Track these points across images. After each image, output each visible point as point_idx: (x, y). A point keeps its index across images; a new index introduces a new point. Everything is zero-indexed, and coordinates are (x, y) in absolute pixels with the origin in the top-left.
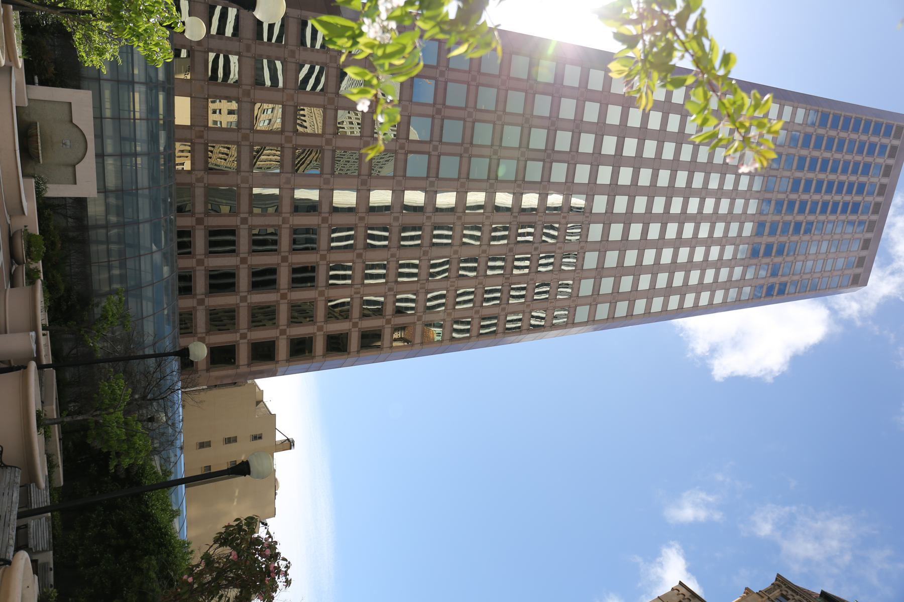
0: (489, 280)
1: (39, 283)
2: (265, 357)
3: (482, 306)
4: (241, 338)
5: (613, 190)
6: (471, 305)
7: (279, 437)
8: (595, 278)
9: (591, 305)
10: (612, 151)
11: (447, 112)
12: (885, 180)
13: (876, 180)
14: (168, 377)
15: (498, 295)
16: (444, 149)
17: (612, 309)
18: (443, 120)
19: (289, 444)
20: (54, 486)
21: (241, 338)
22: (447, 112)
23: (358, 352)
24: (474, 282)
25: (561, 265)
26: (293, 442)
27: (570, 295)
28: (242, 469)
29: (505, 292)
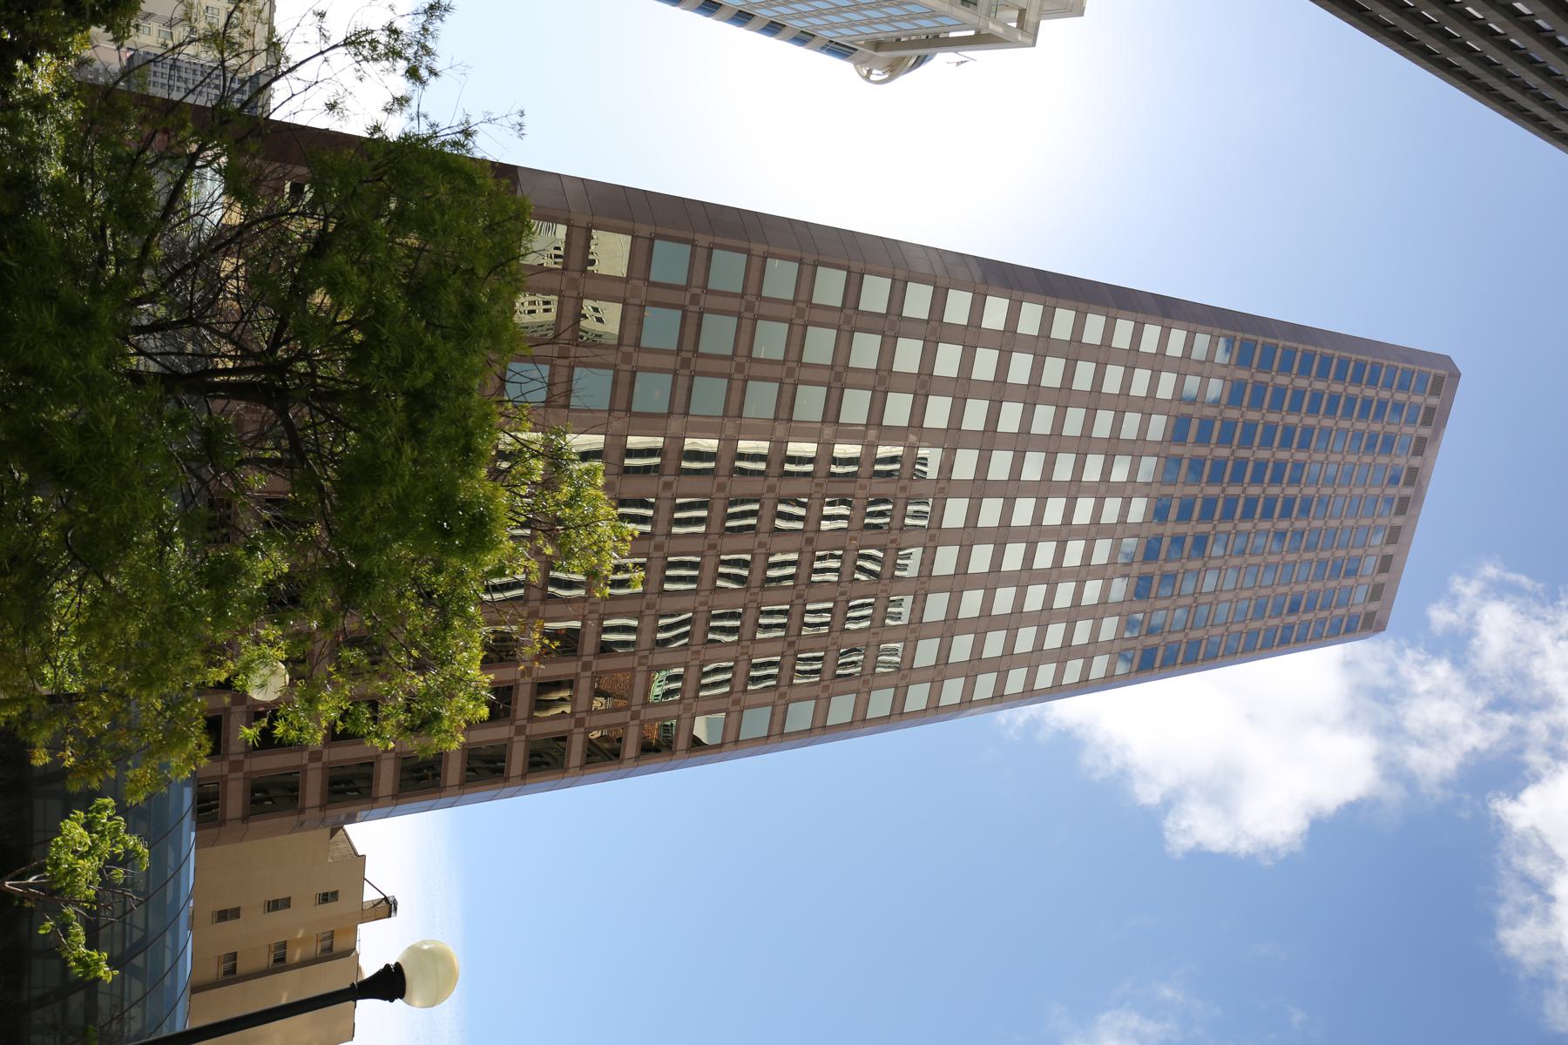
0: (760, 648)
2: (355, 790)
3: (745, 691)
4: (311, 760)
5: (988, 440)
6: (727, 689)
7: (370, 895)
8: (942, 637)
9: (932, 682)
10: (979, 425)
11: (700, 365)
12: (1433, 401)
13: (1403, 461)
15: (775, 671)
16: (712, 301)
17: (969, 687)
18: (692, 378)
19: (387, 907)
21: (311, 760)
22: (700, 365)
23: (523, 776)
24: (733, 651)
25: (905, 516)
26: (395, 903)
27: (898, 668)
29: (787, 666)
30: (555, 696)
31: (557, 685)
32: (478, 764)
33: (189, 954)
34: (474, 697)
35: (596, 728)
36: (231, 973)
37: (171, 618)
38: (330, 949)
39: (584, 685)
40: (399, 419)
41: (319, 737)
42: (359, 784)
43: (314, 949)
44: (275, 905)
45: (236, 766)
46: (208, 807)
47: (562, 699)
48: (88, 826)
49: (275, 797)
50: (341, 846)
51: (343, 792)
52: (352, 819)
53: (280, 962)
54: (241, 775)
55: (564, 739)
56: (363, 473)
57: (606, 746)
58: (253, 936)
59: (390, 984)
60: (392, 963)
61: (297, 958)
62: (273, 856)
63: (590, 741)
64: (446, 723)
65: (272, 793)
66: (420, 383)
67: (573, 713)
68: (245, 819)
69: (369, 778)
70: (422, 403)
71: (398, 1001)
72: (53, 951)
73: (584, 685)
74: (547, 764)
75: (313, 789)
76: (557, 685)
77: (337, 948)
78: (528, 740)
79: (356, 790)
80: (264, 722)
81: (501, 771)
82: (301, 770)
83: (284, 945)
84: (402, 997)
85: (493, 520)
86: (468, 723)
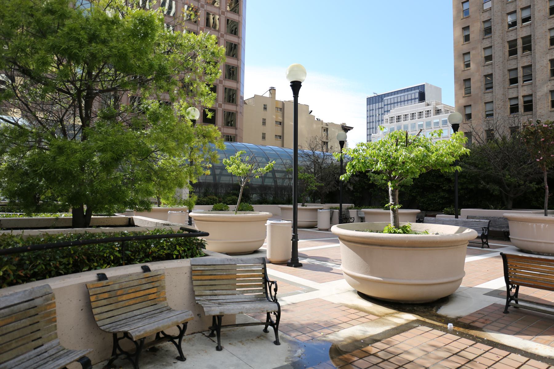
1: (27, 218)
2: (232, 96)
4: (221, 107)
7: (267, 95)
14: (284, 161)
19: (272, 90)
20: (71, 225)
21: (221, 107)
23: (239, 38)
28: (326, 130)
30: (211, 21)
31: (208, 20)
32: (231, 53)
33: (272, 146)
34: (208, 39)
35: (226, 8)
36: (281, 137)
37: (170, 131)
38: (281, 109)
39: (209, 8)
40: (100, 46)
41: (214, 94)
42: (231, 94)
43: (280, 114)
44: (264, 123)
45: (220, 106)
46: (230, 139)
47: (214, 19)
48: (230, 166)
49: (230, 119)
50: (250, 101)
51: (233, 99)
52: (242, 98)
53: (281, 123)
54: (223, 105)
55: (228, 20)
56: (122, 63)
57: (233, 5)
58: (272, 130)
59: (296, 86)
60: (290, 84)
61: (281, 119)
62: (248, 122)
63: (231, 11)
64: (215, 50)
65: (229, 120)
66: (86, 37)
67: (219, 15)
68: (236, 129)
69: (230, 90)
70: (93, 38)
71: (302, 84)
72: (264, 177)
73: (209, 8)
74: (236, 28)
75: (230, 107)
76: (208, 20)
77: (281, 108)
78: (226, 33)
79: (233, 95)
80: (207, 110)
81: (235, 45)
82: (224, 111)
83: (276, 122)
84: (301, 83)
85: (142, 16)
86: (216, 43)
